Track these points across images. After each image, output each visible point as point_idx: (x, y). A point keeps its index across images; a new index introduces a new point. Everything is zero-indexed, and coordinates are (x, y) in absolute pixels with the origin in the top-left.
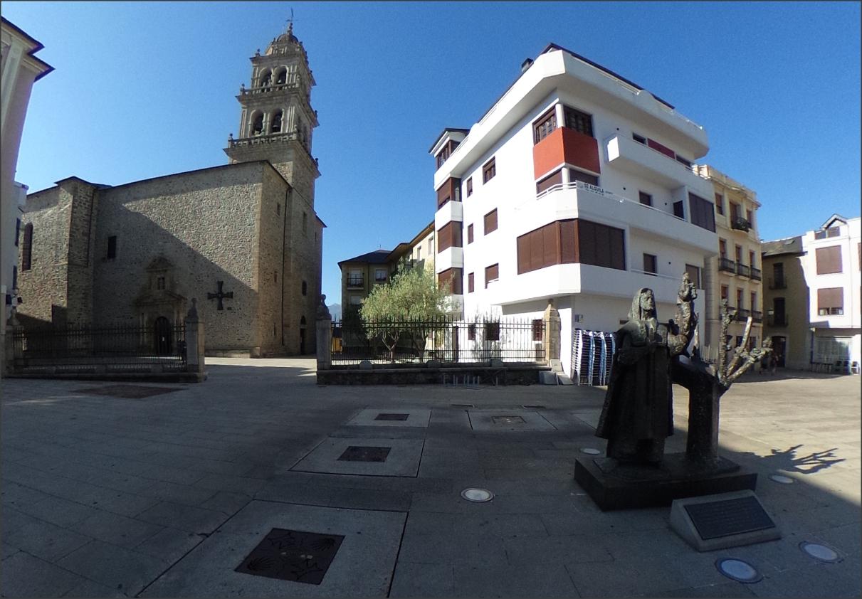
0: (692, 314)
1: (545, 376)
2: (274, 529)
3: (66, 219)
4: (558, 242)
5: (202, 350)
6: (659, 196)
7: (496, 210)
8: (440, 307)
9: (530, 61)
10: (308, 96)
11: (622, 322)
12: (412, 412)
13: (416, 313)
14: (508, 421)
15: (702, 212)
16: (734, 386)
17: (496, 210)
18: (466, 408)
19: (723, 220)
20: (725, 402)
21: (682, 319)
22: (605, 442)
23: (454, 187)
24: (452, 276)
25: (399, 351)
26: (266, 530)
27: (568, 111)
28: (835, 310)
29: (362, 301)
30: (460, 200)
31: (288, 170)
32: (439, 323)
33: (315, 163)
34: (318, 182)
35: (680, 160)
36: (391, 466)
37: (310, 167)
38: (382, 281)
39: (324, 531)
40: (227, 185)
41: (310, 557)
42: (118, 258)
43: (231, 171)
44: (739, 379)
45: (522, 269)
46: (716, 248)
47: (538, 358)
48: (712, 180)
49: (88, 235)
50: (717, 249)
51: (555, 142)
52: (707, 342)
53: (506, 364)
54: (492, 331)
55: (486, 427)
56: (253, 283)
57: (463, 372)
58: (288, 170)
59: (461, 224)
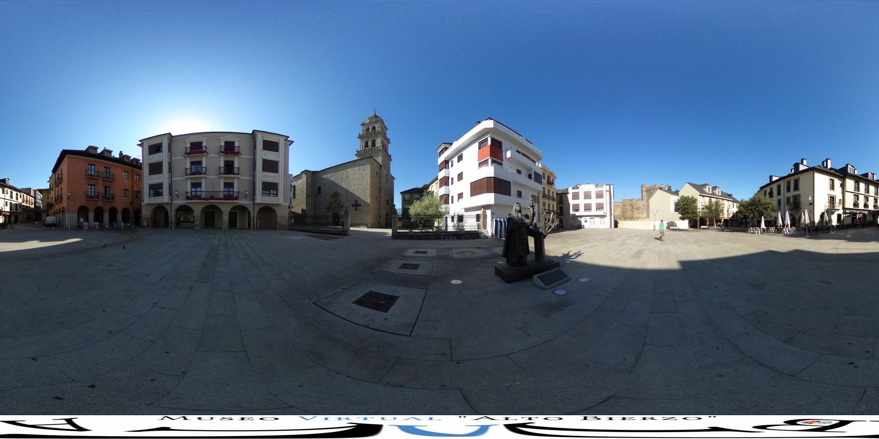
0: (534, 211)
1: (482, 236)
2: (371, 291)
3: (305, 182)
4: (486, 185)
5: (349, 225)
6: (523, 171)
7: (462, 172)
8: (440, 209)
9: (479, 122)
10: (385, 134)
11: (509, 215)
12: (429, 250)
13: (431, 212)
14: (468, 253)
15: (538, 178)
16: (548, 235)
17: (462, 172)
18: (451, 249)
19: (545, 181)
20: (546, 240)
21: (530, 213)
22: (506, 259)
23: (446, 164)
24: (445, 197)
25: (424, 227)
26: (367, 291)
27: (493, 140)
28: (577, 210)
29: (410, 207)
30: (448, 168)
31: (380, 159)
32: (440, 215)
33: (390, 156)
34: (391, 163)
35: (532, 160)
36: (419, 271)
37: (389, 158)
38: (417, 199)
39: (391, 294)
40: (357, 167)
41: (384, 303)
42: (322, 193)
43: (358, 162)
44: (550, 233)
45: (472, 195)
46: (542, 190)
47: (478, 229)
48: (542, 168)
49: (312, 187)
50: (542, 190)
51: (487, 149)
52: (539, 221)
53: (466, 231)
54: (461, 218)
55: (459, 256)
56: (368, 200)
57: (449, 235)
58: (380, 159)
59: (448, 177)
